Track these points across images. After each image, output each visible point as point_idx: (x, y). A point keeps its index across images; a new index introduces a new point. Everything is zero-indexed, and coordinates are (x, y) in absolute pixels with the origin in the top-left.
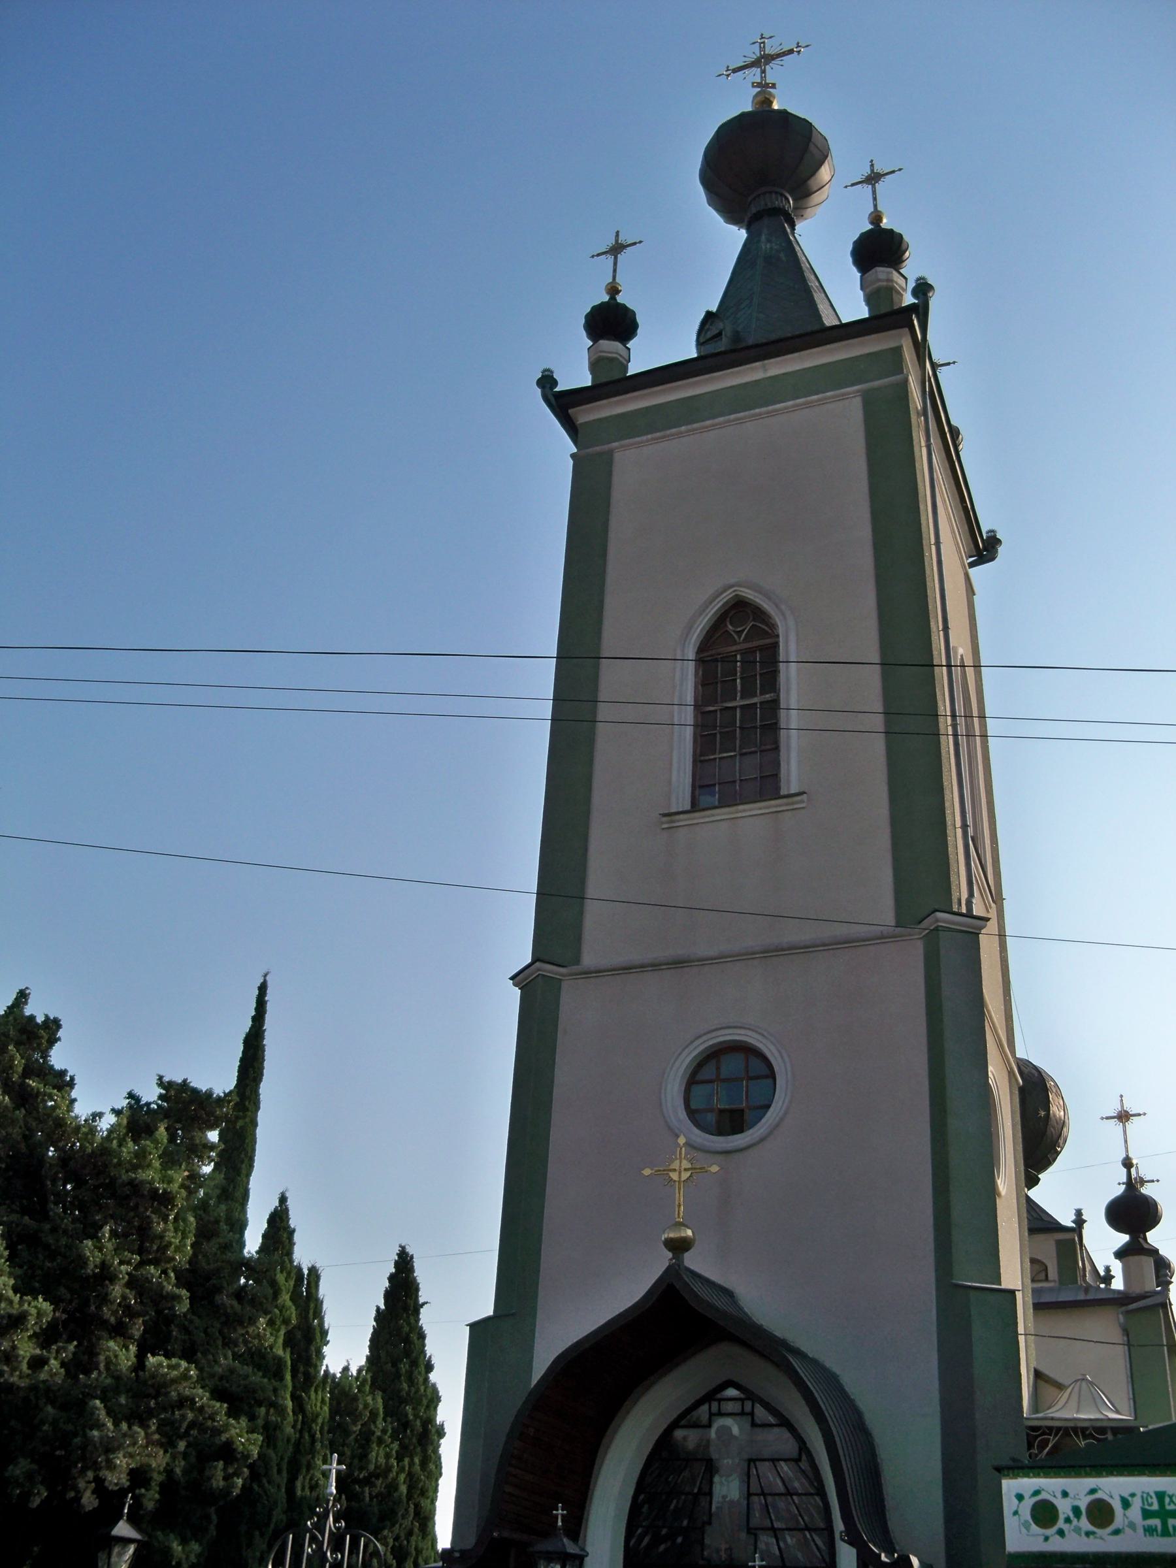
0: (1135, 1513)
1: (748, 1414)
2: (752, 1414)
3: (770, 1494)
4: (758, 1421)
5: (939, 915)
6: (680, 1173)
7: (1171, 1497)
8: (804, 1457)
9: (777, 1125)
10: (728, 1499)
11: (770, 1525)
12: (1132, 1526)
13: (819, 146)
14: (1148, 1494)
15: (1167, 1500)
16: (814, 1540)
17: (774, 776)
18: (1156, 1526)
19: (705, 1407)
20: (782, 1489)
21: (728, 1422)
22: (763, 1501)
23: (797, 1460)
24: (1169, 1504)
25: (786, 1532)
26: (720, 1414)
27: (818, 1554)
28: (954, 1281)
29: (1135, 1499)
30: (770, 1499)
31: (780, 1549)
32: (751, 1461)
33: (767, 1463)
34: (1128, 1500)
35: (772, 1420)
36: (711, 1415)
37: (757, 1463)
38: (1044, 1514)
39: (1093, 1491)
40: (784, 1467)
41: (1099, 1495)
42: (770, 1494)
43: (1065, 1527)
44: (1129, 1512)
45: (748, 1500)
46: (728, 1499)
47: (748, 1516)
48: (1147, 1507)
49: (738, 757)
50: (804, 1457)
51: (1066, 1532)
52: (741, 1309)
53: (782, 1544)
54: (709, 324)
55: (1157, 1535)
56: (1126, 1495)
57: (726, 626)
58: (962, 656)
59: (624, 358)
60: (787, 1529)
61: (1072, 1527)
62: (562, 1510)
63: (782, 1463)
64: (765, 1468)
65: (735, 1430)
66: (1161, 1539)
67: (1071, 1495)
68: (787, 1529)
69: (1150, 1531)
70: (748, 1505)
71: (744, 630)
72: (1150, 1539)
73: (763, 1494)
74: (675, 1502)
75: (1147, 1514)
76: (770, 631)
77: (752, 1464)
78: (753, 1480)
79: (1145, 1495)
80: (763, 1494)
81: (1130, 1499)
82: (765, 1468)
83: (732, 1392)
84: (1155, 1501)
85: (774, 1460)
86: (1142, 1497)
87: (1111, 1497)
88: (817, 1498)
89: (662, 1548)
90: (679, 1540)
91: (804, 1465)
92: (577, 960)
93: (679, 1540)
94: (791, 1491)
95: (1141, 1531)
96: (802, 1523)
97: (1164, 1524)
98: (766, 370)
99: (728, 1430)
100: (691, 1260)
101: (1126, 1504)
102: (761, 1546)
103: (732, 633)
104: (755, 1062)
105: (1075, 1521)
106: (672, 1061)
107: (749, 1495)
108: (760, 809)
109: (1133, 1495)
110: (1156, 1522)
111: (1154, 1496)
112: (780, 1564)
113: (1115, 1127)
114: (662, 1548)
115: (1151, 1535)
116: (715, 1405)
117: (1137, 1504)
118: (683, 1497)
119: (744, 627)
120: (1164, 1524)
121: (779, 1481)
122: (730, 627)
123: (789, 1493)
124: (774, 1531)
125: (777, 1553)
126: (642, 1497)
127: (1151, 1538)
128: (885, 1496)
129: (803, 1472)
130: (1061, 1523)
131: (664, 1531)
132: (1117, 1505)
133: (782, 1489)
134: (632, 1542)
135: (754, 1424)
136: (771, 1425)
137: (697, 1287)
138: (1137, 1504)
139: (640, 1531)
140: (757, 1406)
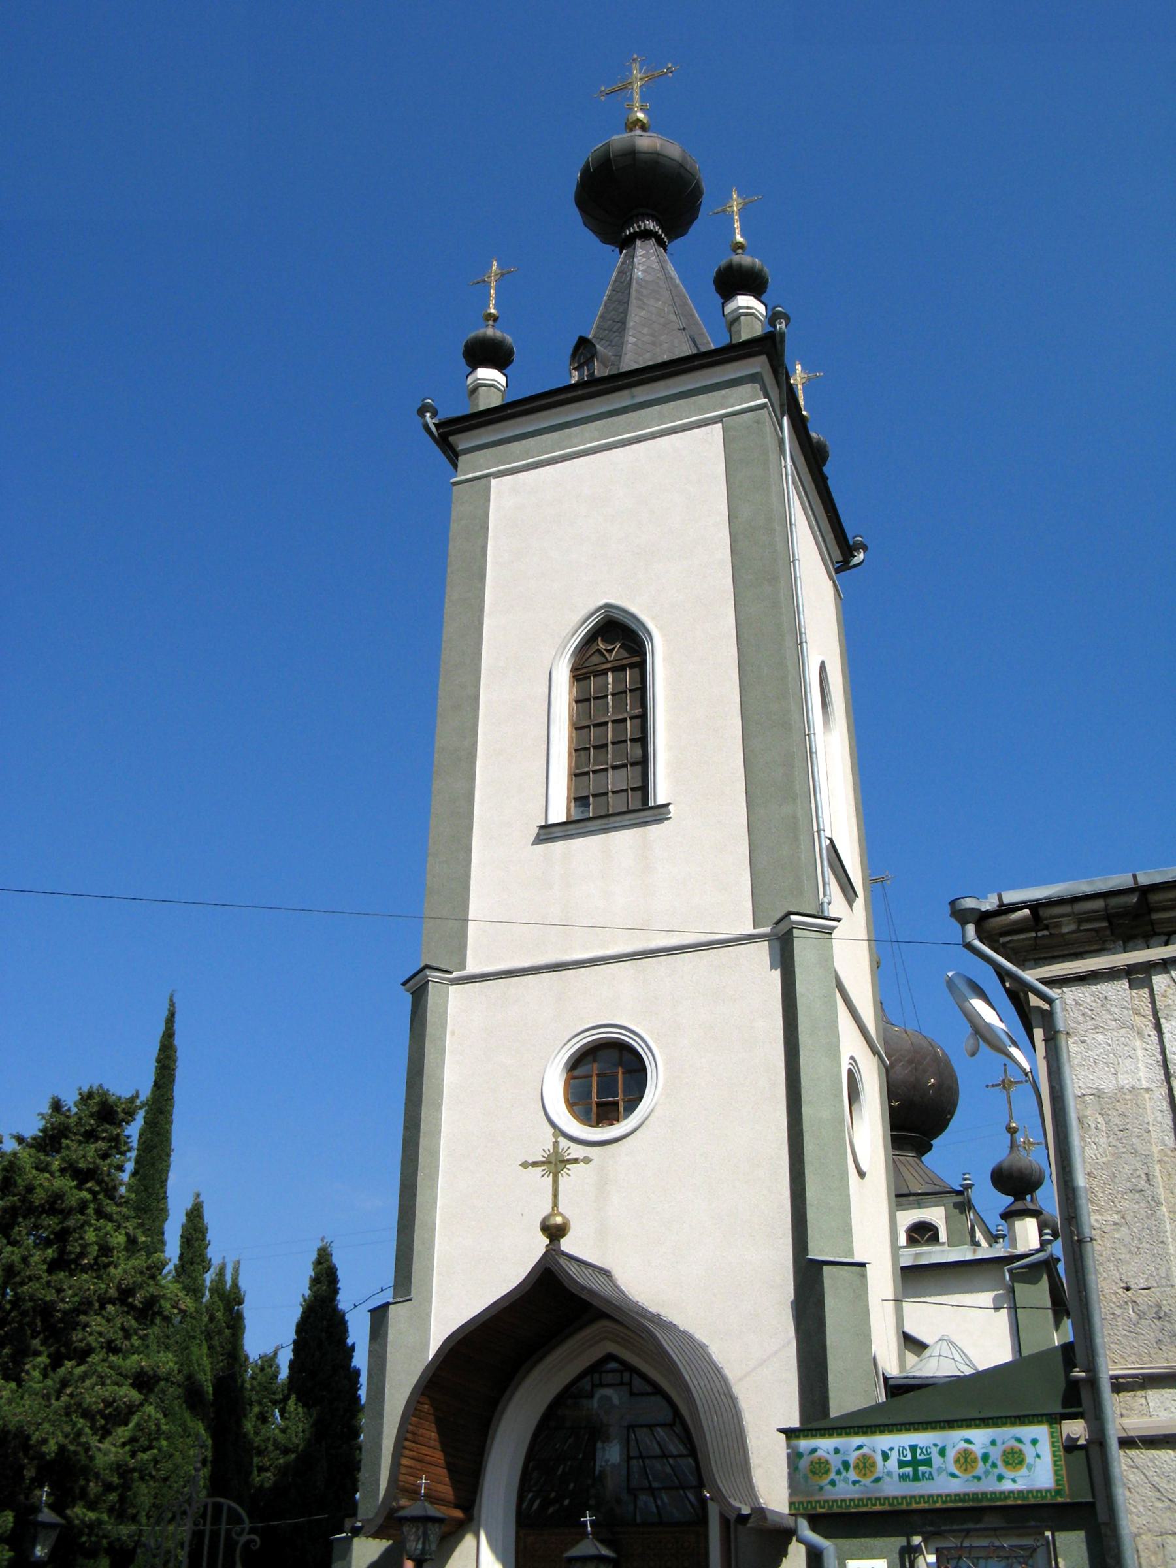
0: (892, 1463)
1: (627, 1384)
2: (630, 1384)
3: (648, 1457)
4: (635, 1391)
5: (793, 917)
6: (556, 1164)
7: (921, 1449)
8: (678, 1421)
9: (646, 1119)
10: (610, 1463)
11: (647, 1484)
12: (889, 1474)
13: (688, 168)
14: (904, 1448)
15: (919, 1451)
16: (687, 1497)
17: (643, 788)
18: (909, 1473)
19: (588, 1378)
20: (658, 1452)
21: (608, 1392)
22: (641, 1464)
23: (671, 1425)
24: (920, 1455)
25: (663, 1491)
26: (601, 1385)
27: (692, 1511)
28: (809, 1257)
29: (893, 1452)
30: (647, 1461)
31: (657, 1506)
32: (631, 1427)
33: (645, 1429)
34: (887, 1454)
35: (649, 1389)
36: (593, 1386)
37: (636, 1429)
38: (1014, 1458)
39: (860, 1447)
40: (660, 1431)
41: (865, 1450)
42: (648, 1457)
43: (836, 1478)
44: (888, 1463)
45: (628, 1464)
46: (610, 1463)
47: (628, 1480)
48: (902, 1458)
49: (610, 771)
50: (678, 1421)
51: (837, 1482)
52: (618, 1287)
53: (659, 1503)
54: (582, 348)
55: (909, 1480)
56: (886, 1449)
57: (598, 645)
58: (823, 666)
59: (502, 385)
60: (664, 1488)
61: (842, 1477)
62: (425, 1480)
63: (659, 1429)
64: (643, 1434)
65: (616, 1400)
66: (911, 1483)
67: (842, 1452)
68: (664, 1488)
69: (903, 1477)
70: (628, 1468)
71: (614, 649)
72: (903, 1484)
73: (641, 1457)
74: (562, 1467)
75: (902, 1464)
76: (638, 649)
77: (631, 1430)
78: (633, 1444)
79: (901, 1449)
80: (641, 1457)
81: (889, 1452)
82: (643, 1434)
83: (613, 1365)
84: (909, 1453)
85: (651, 1426)
86: (899, 1451)
87: (874, 1451)
88: (690, 1460)
89: (551, 1510)
90: (566, 1502)
91: (678, 1429)
92: (463, 966)
93: (566, 1502)
94: (644, 1454)
95: (896, 1477)
96: (676, 1481)
97: (915, 1471)
98: (633, 397)
99: (608, 1398)
100: (566, 1245)
101: (886, 1457)
102: (640, 1504)
103: (604, 652)
104: (627, 1056)
105: (844, 1473)
106: (553, 1056)
107: (629, 1458)
108: (630, 820)
109: (891, 1449)
110: (908, 1470)
111: (908, 1450)
112: (1057, 1534)
113: (999, 1094)
114: (551, 1510)
115: (905, 1480)
116: (596, 1376)
117: (894, 1456)
118: (569, 1463)
119: (612, 647)
120: (915, 1471)
121: (656, 1446)
122: (601, 645)
123: (665, 1455)
124: (652, 1491)
125: (655, 1510)
126: (531, 1465)
127: (905, 1483)
128: (750, 1455)
129: (677, 1435)
130: (832, 1475)
131: (553, 1495)
132: (879, 1458)
133: (658, 1452)
134: (524, 1506)
135: (632, 1394)
136: (648, 1394)
137: (572, 1269)
138: (894, 1456)
139: (530, 1495)
140: (635, 1376)
